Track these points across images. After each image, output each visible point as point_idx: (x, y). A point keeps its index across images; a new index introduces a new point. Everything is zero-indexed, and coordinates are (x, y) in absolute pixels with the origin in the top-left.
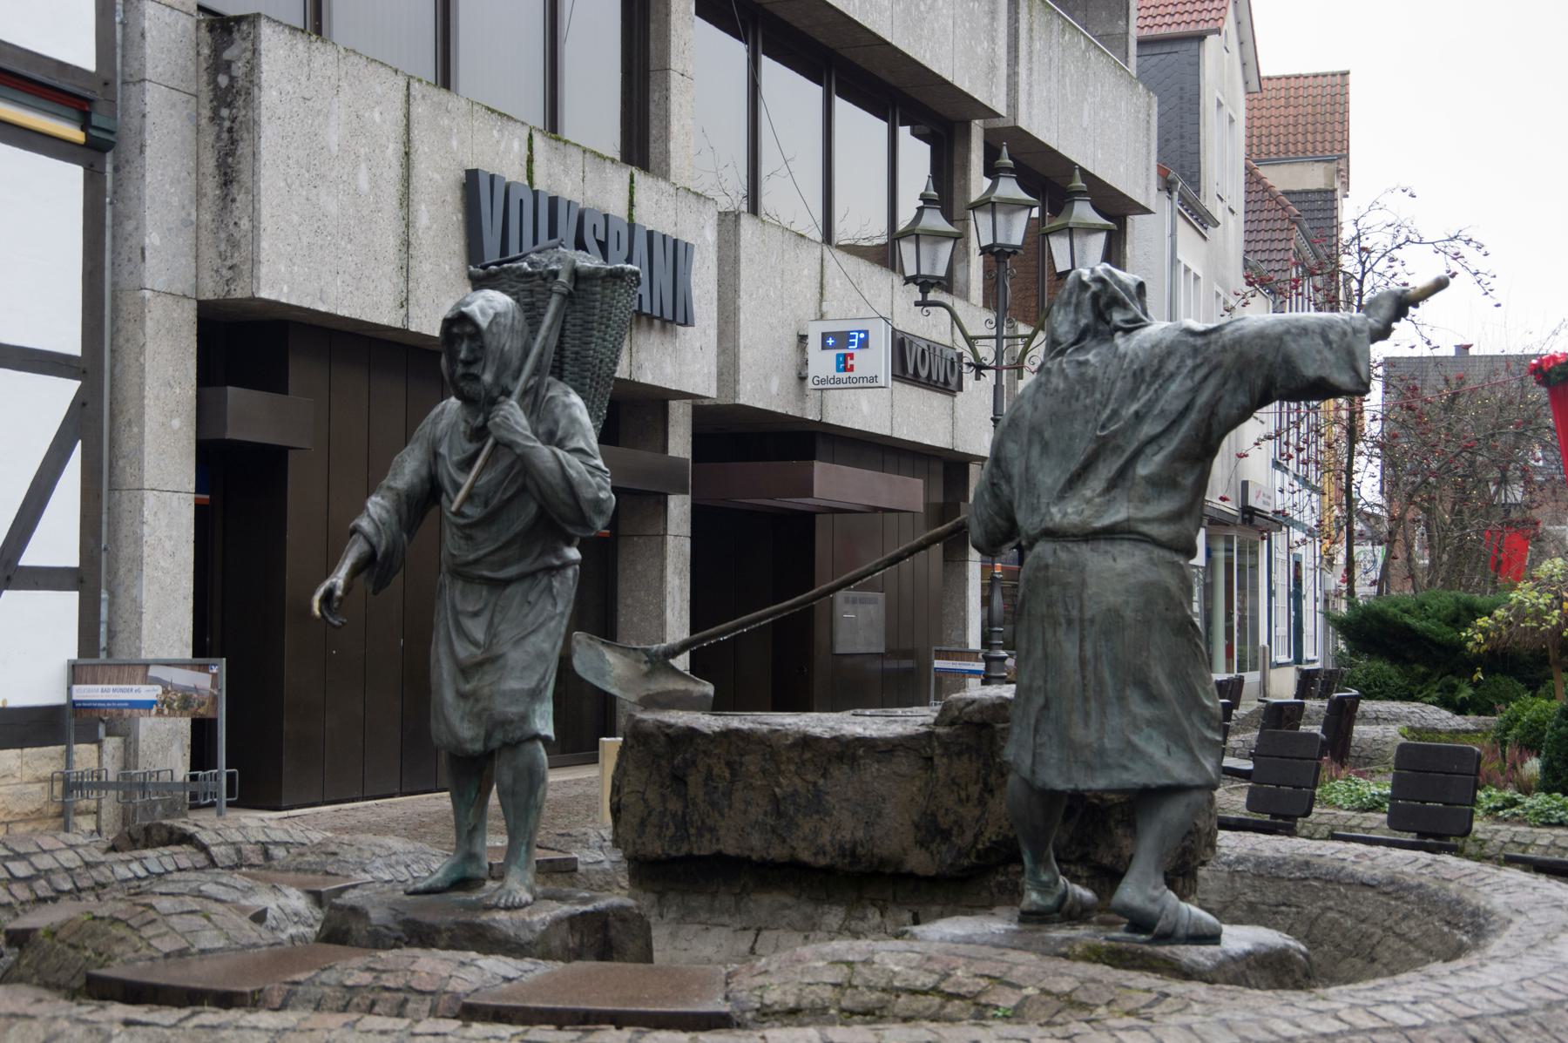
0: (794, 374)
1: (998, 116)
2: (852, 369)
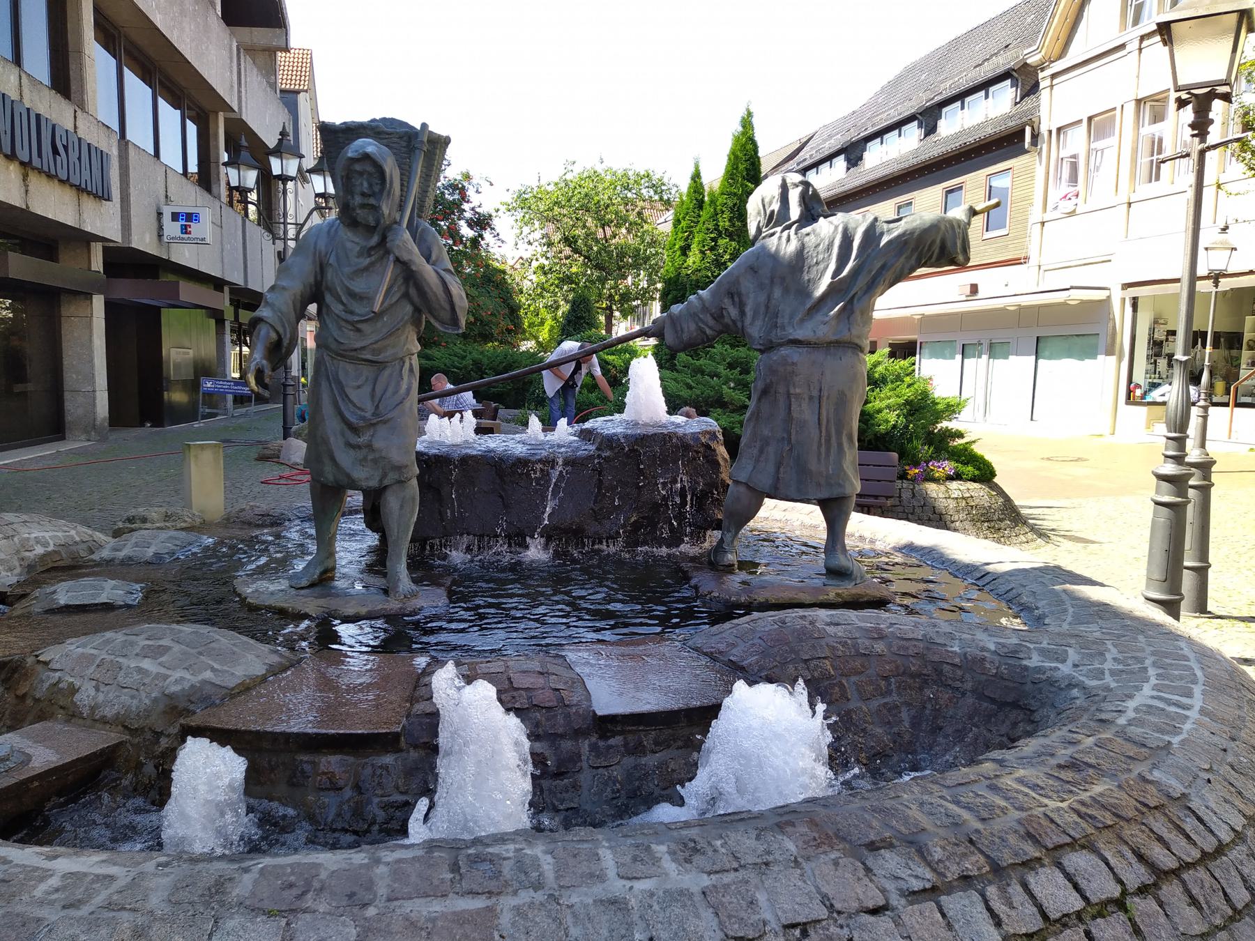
0: (156, 233)
1: (234, 111)
2: (190, 233)
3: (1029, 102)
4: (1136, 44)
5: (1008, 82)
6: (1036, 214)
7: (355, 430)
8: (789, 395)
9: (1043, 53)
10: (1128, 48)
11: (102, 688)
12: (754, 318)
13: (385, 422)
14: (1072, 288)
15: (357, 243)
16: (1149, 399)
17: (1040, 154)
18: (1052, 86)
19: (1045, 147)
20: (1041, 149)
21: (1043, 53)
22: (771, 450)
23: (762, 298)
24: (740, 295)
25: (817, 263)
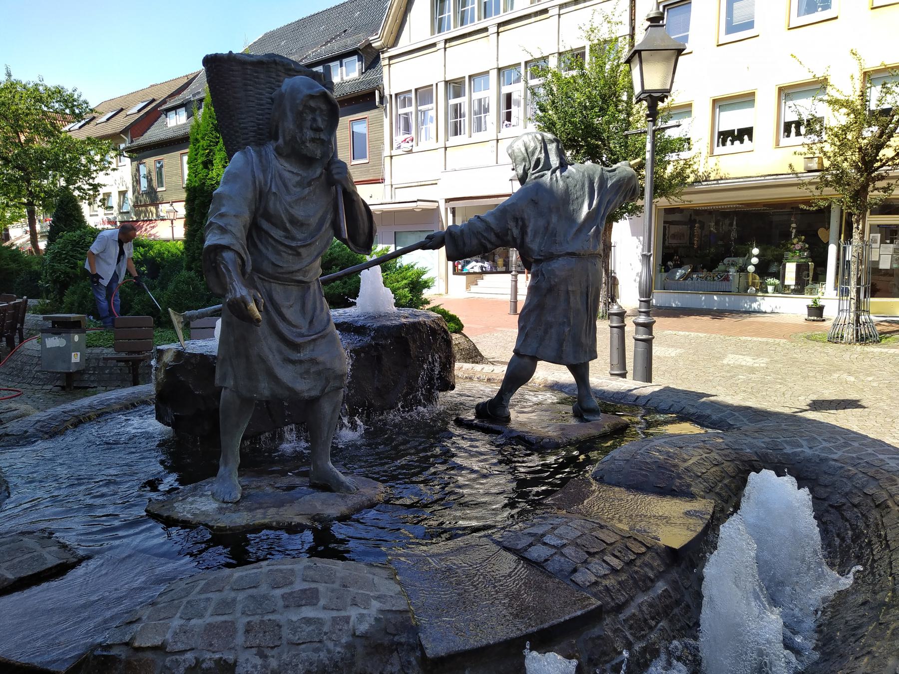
3: (371, 75)
4: (441, 45)
5: (356, 57)
6: (387, 152)
7: (296, 347)
8: (567, 292)
9: (383, 41)
10: (438, 47)
11: (269, 653)
12: (535, 236)
13: (323, 337)
14: (418, 200)
15: (297, 174)
16: (464, 271)
17: (385, 110)
18: (389, 65)
19: (388, 105)
20: (386, 106)
21: (383, 41)
22: (553, 331)
23: (541, 222)
24: (523, 220)
25: (577, 198)
